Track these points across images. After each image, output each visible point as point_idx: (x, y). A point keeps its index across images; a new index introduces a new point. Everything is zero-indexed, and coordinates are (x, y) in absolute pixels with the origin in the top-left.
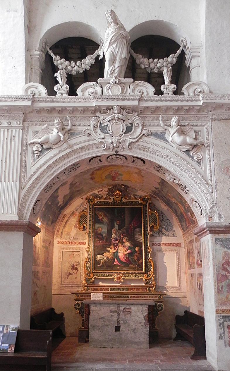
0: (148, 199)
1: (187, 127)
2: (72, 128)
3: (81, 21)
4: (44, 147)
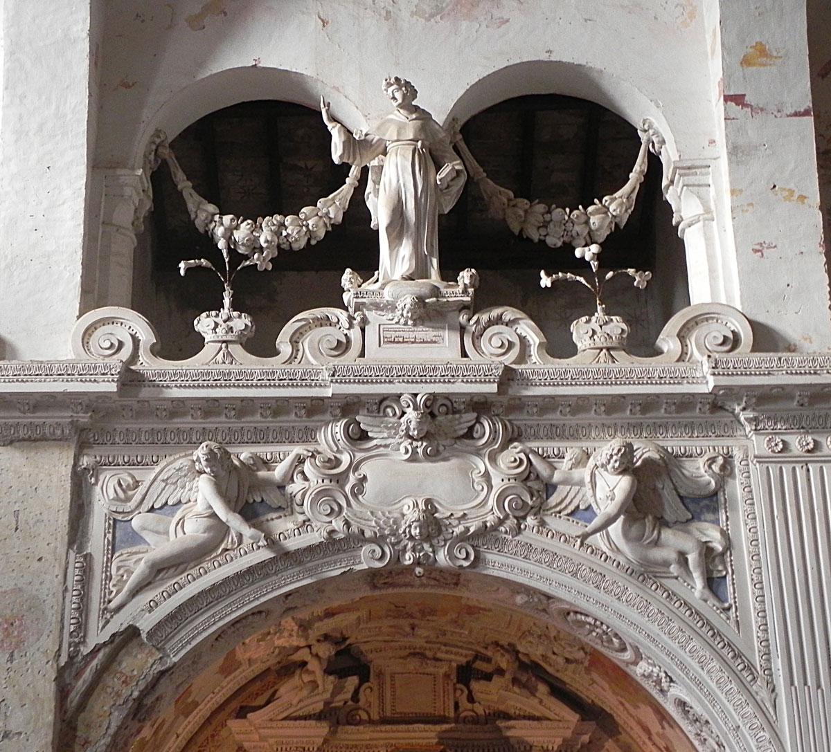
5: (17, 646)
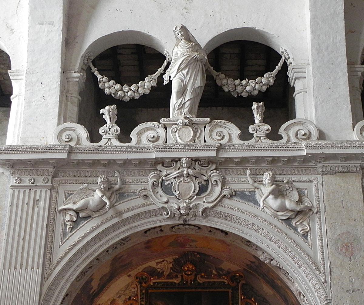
0: (241, 276)
1: (286, 185)
2: (123, 186)
3: (139, 30)
4: (81, 216)
5: (352, 255)
